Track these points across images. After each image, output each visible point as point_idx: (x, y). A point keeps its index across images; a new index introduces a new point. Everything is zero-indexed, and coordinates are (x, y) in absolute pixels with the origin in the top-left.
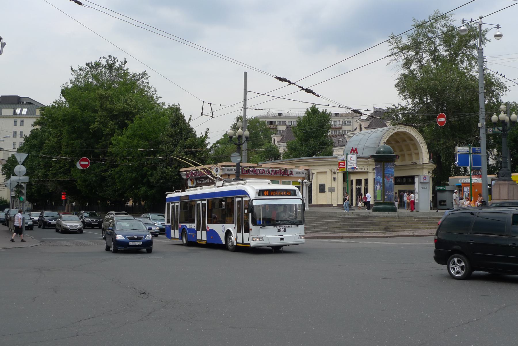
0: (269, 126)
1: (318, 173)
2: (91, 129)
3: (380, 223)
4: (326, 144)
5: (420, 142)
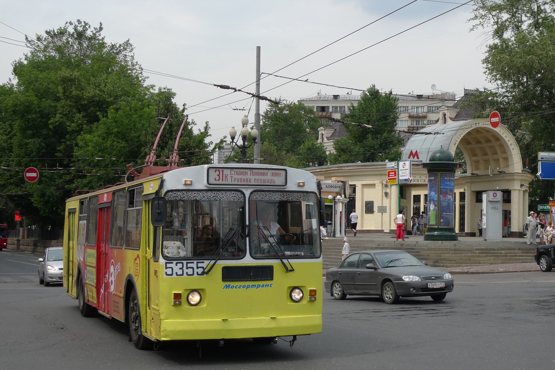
0: (320, 114)
1: (364, 186)
2: (52, 124)
3: (428, 256)
4: (391, 142)
5: (509, 144)
